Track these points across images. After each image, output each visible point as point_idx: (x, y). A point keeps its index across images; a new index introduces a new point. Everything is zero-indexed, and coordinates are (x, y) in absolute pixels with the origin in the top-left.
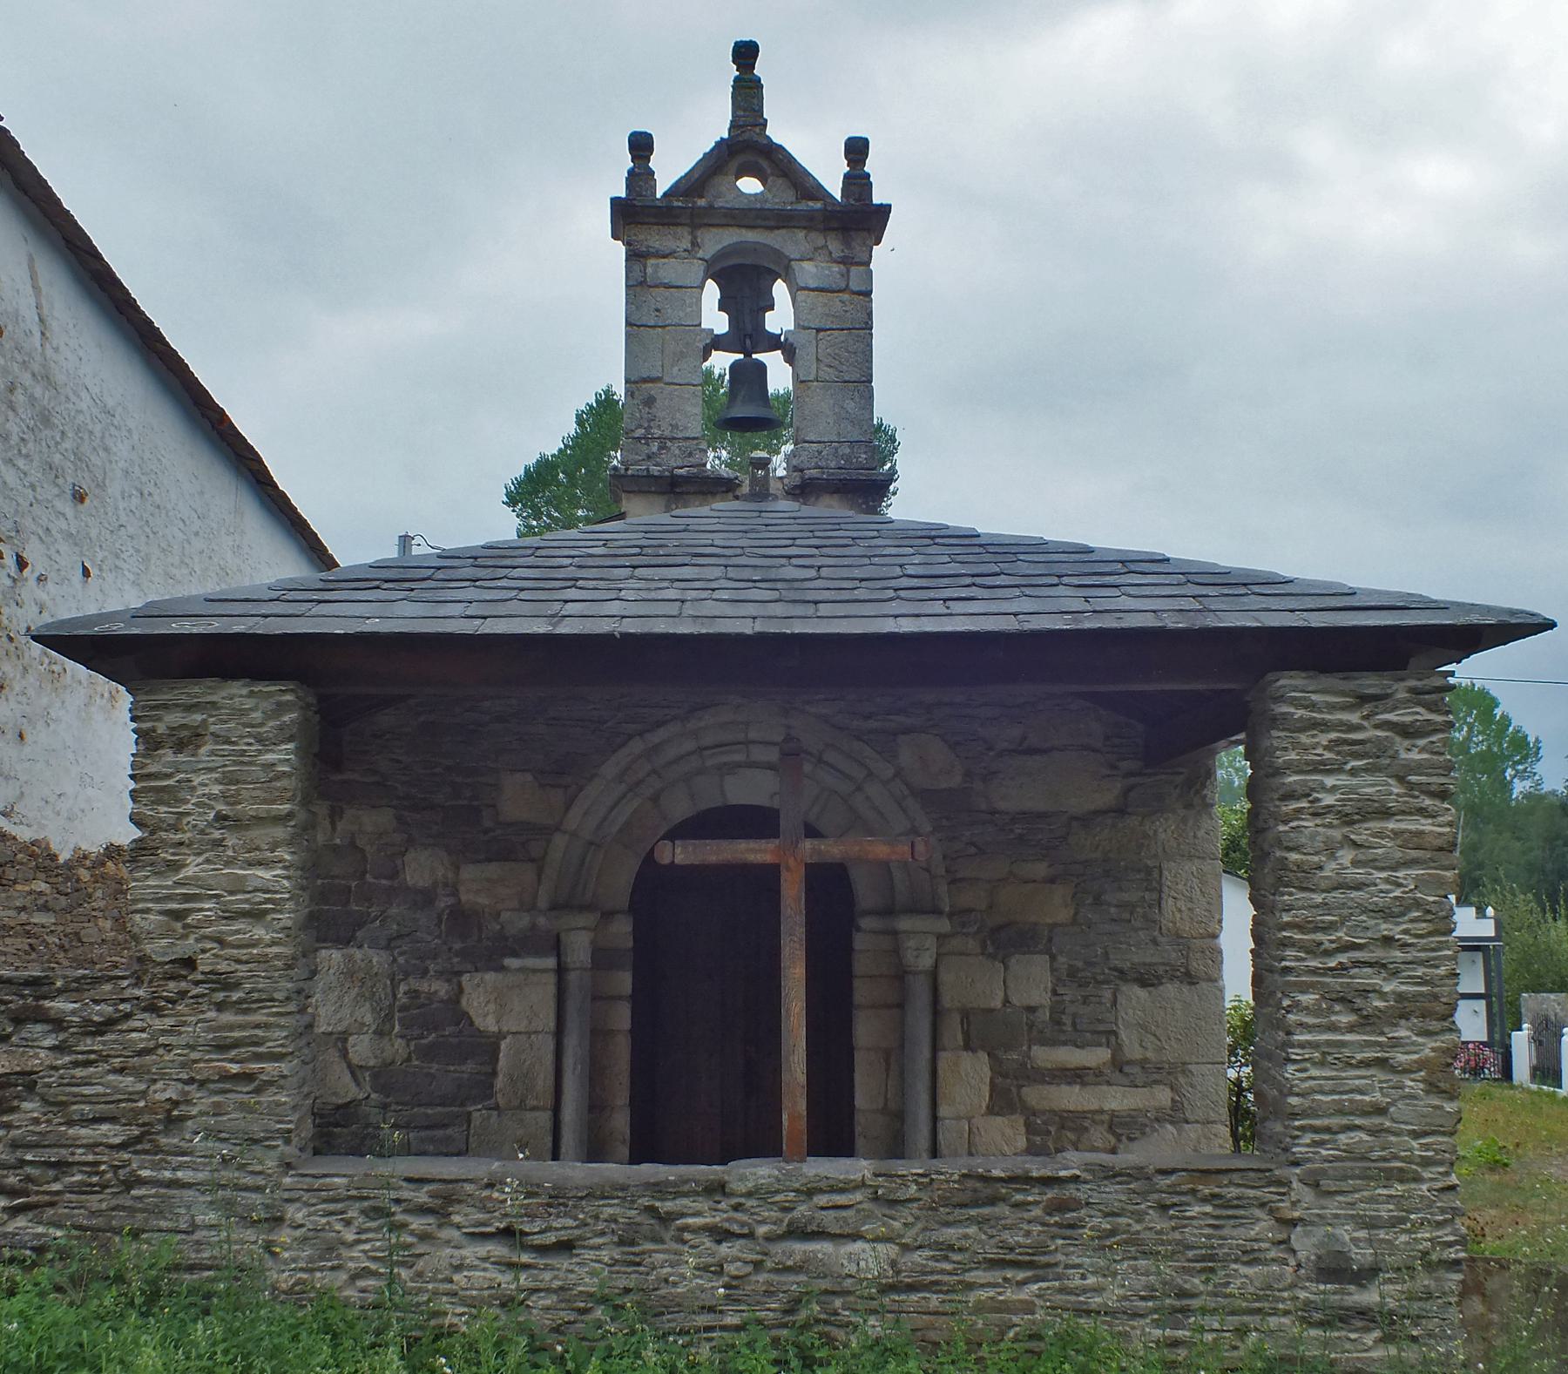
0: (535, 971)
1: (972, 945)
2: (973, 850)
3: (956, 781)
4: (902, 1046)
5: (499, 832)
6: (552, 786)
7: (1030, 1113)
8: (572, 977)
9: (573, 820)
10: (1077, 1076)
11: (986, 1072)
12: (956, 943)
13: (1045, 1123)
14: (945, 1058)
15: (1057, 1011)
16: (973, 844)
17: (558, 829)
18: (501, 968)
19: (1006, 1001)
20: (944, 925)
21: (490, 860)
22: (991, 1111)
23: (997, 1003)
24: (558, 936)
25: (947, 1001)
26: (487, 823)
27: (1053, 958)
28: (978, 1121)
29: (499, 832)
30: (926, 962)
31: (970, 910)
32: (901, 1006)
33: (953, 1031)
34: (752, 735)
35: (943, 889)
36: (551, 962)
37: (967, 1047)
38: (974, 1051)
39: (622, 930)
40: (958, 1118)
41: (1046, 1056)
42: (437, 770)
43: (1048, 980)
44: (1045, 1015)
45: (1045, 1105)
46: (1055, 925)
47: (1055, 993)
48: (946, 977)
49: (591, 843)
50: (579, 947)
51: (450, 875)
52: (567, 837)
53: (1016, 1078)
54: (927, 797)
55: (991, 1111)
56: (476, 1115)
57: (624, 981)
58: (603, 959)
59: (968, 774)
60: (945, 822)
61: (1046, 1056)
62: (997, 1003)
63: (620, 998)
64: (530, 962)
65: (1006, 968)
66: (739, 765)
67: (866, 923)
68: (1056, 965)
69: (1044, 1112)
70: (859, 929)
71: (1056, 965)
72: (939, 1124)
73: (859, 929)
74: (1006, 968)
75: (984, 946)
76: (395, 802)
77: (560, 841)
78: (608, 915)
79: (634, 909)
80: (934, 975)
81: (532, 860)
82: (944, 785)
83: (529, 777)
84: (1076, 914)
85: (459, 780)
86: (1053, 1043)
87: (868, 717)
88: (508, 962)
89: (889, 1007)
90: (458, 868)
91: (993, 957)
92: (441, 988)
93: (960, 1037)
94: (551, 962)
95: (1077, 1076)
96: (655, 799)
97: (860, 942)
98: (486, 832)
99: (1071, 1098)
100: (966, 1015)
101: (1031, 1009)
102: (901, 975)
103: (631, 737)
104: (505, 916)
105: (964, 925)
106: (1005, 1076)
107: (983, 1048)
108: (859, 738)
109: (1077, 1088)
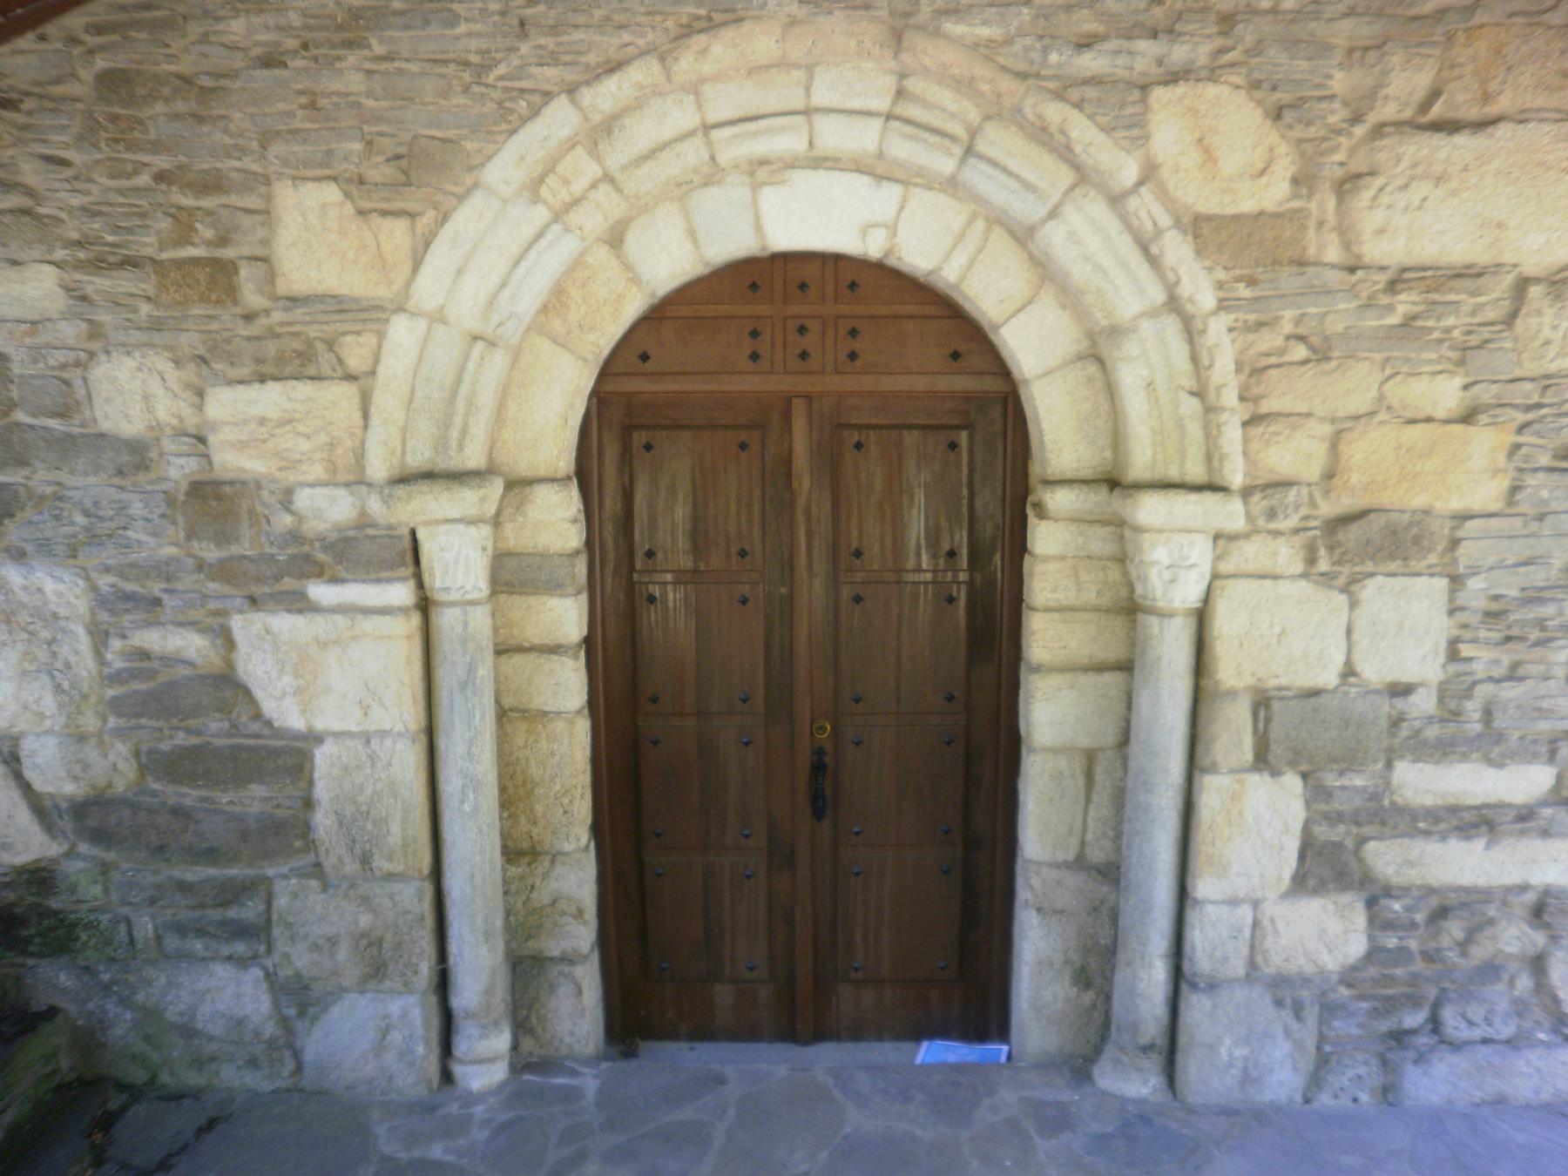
0: (367, 611)
1: (1287, 556)
2: (1301, 352)
3: (1274, 193)
4: (1125, 740)
5: (277, 316)
6: (385, 213)
7: (1376, 895)
8: (447, 621)
9: (429, 287)
10: (1480, 822)
11: (1296, 812)
12: (1251, 554)
13: (1408, 909)
14: (1213, 792)
15: (1451, 695)
16: (1301, 338)
17: (401, 309)
18: (300, 604)
19: (1349, 672)
20: (1231, 513)
21: (262, 380)
22: (1301, 884)
23: (1328, 677)
24: (413, 533)
25: (1231, 670)
26: (252, 297)
27: (1456, 581)
28: (1276, 910)
29: (277, 316)
30: (1188, 593)
31: (1286, 484)
32: (1126, 667)
33: (1233, 732)
34: (821, 97)
35: (1232, 436)
36: (401, 593)
37: (1262, 760)
38: (1275, 773)
39: (556, 520)
40: (1233, 902)
41: (1419, 782)
42: (144, 179)
43: (1440, 628)
44: (1423, 703)
45: (1413, 876)
46: (1464, 517)
47: (1453, 655)
48: (1224, 624)
49: (476, 338)
50: (459, 561)
51: (187, 412)
52: (422, 325)
53: (1358, 824)
54: (1203, 230)
55: (1301, 884)
56: (279, 886)
57: (566, 616)
58: (512, 575)
59: (1303, 182)
60: (1244, 291)
61: (1419, 782)
62: (1328, 677)
63: (554, 649)
64: (354, 593)
65: (1354, 604)
66: (793, 164)
67: (1059, 500)
68: (1462, 598)
69: (1406, 890)
70: (1042, 514)
71: (1462, 598)
72: (1192, 917)
73: (1042, 514)
74: (1354, 604)
75: (1311, 560)
76: (60, 254)
77: (402, 332)
78: (518, 485)
79: (585, 475)
80: (1202, 617)
81: (351, 378)
82: (1247, 206)
83: (332, 193)
84: (1515, 489)
85: (188, 201)
86: (1443, 751)
87: (1085, 44)
88: (320, 592)
89: (1099, 668)
90: (201, 394)
91: (1327, 579)
92: (192, 645)
93: (1248, 741)
94: (401, 593)
95: (1480, 822)
96: (615, 239)
97: (1045, 538)
98: (249, 317)
99: (1462, 864)
100: (1262, 703)
101: (1400, 690)
102: (1130, 609)
103: (548, 96)
104: (303, 499)
105: (1272, 514)
106: (1334, 818)
107: (1292, 764)
108: (1059, 95)
109: (1479, 844)
